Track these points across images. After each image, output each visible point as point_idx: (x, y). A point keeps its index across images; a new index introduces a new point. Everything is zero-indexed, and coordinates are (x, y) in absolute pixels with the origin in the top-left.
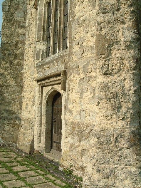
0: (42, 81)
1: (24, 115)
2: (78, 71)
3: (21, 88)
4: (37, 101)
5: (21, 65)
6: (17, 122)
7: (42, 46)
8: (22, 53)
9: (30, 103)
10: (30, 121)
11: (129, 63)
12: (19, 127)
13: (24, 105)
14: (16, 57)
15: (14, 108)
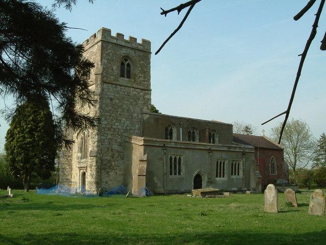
0: (80, 168)
1: (73, 180)
2: (206, 218)
3: (72, 169)
4: (78, 175)
5: (71, 160)
6: (70, 183)
7: (80, 155)
8: (72, 155)
9: (75, 175)
10: (76, 182)
11: (95, 169)
12: (71, 185)
13: (73, 176)
14: (69, 157)
15: (69, 177)
